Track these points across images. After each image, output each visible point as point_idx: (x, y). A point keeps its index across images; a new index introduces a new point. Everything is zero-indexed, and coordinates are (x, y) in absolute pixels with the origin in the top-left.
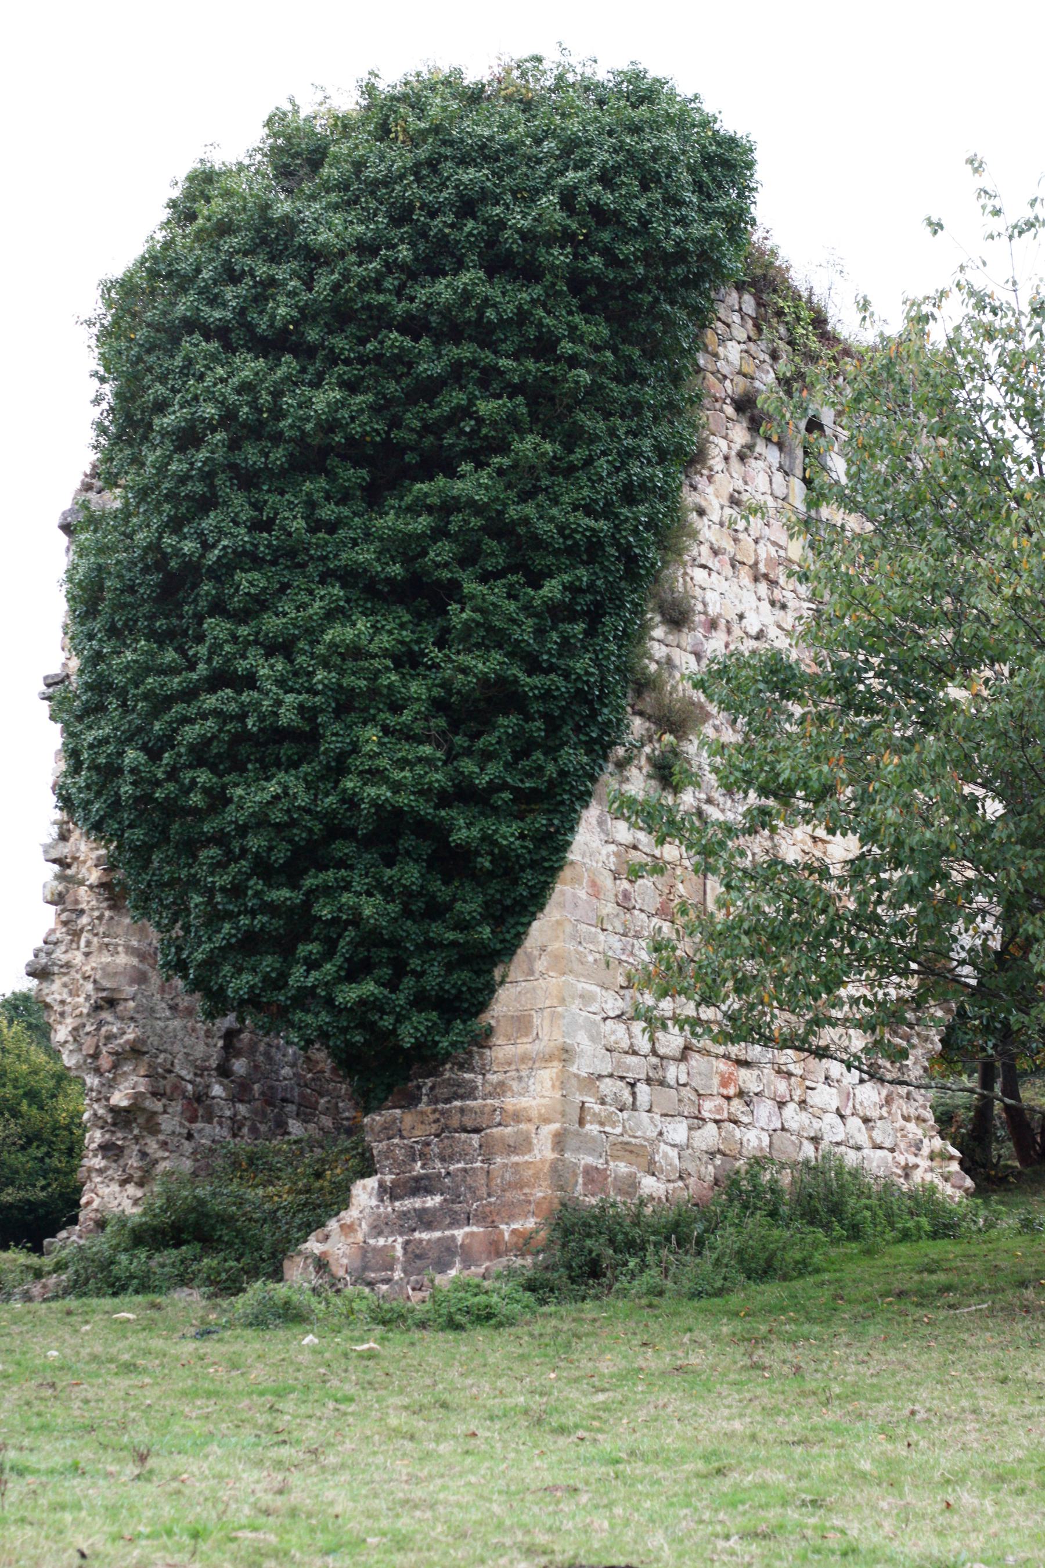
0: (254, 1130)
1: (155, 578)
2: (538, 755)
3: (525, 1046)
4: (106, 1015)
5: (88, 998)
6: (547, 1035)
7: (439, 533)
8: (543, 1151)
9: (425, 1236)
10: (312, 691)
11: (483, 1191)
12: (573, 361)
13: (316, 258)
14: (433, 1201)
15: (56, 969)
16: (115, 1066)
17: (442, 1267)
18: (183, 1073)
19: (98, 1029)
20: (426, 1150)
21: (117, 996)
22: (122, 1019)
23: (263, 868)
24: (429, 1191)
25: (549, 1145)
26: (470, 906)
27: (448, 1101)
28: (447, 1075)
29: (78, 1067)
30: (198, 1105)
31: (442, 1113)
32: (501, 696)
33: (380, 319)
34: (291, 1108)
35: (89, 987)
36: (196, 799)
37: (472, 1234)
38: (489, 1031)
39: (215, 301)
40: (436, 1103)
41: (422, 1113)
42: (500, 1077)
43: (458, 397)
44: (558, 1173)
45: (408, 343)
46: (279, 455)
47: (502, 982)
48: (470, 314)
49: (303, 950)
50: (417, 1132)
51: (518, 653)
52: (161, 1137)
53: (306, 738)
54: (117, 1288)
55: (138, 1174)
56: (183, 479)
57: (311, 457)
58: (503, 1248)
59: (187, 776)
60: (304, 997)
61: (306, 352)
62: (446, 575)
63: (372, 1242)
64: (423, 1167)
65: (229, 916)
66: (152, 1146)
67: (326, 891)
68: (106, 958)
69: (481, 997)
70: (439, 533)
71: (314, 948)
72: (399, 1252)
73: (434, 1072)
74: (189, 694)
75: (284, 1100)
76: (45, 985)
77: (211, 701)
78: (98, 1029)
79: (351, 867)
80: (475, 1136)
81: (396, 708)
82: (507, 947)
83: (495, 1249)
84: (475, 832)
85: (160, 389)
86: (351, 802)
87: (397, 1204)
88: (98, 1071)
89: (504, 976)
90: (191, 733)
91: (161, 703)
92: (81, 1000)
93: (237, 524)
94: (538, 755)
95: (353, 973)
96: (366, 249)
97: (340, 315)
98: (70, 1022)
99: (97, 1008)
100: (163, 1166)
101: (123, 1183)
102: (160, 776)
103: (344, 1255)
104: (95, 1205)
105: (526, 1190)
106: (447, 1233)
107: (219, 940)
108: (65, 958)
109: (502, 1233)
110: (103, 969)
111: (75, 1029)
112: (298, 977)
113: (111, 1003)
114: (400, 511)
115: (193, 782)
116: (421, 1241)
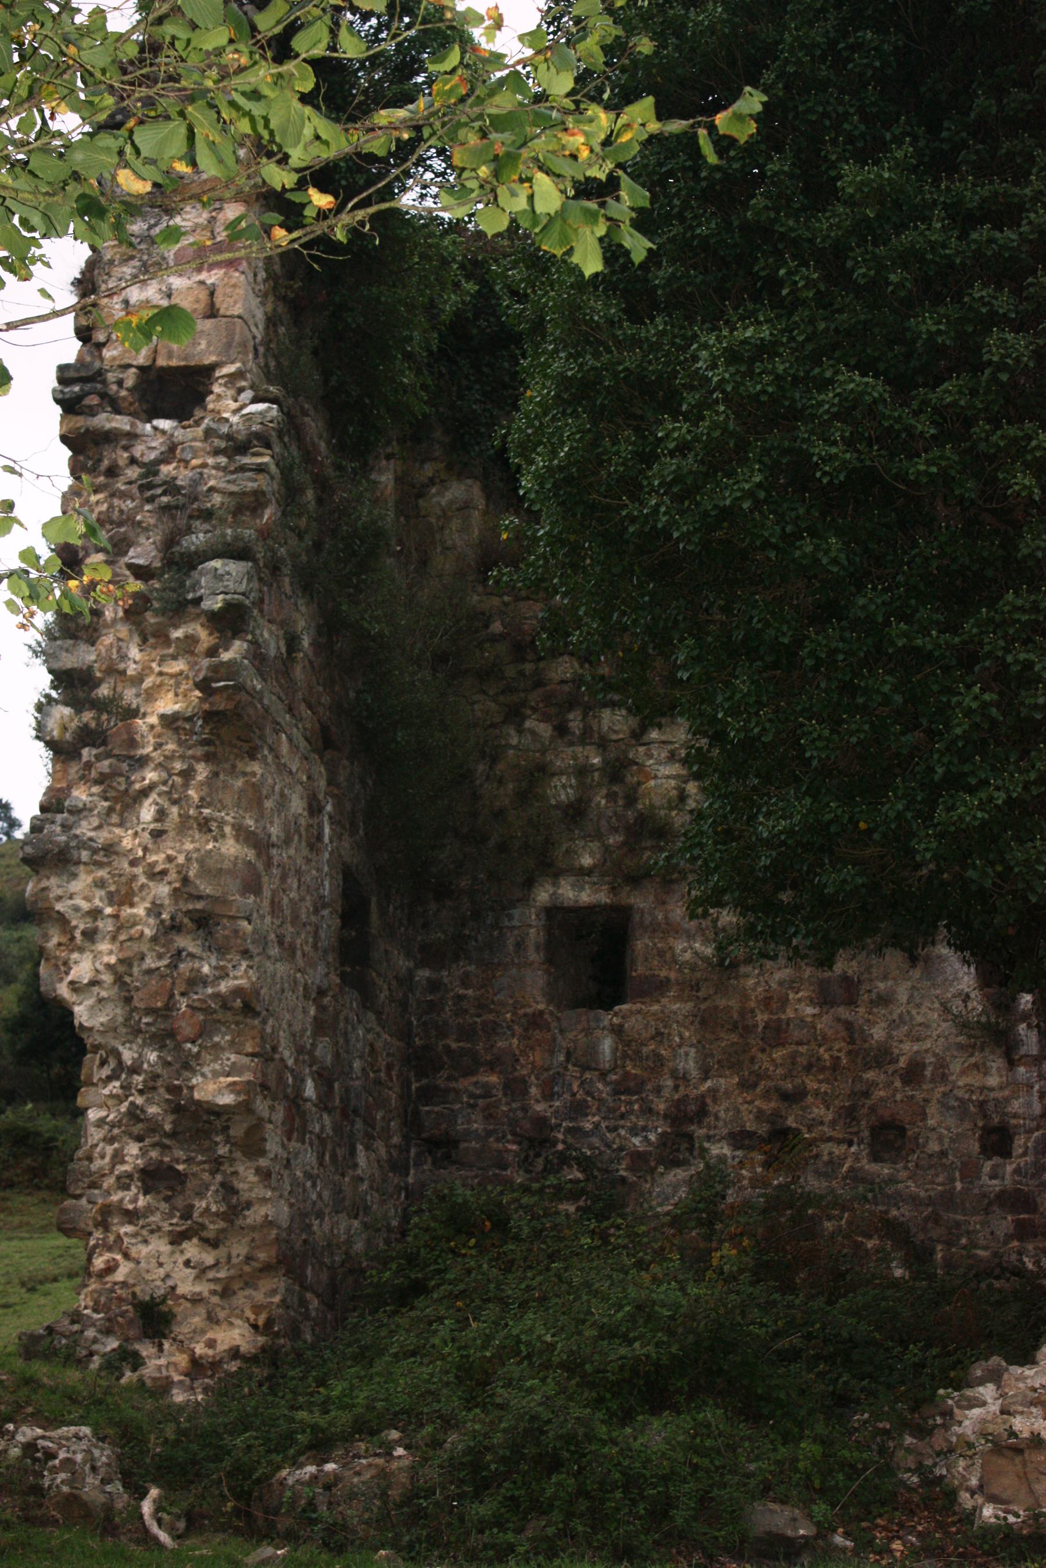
4: (187, 943)
5: (155, 910)
15: (85, 855)
16: (203, 1032)
21: (219, 909)
22: (222, 951)
29: (111, 1029)
35: (163, 890)
52: (263, 1162)
55: (213, 1227)
78: (173, 966)
88: (164, 1038)
98: (107, 952)
100: (255, 1215)
101: (177, 1239)
104: (120, 1275)
108: (103, 837)
110: (201, 861)
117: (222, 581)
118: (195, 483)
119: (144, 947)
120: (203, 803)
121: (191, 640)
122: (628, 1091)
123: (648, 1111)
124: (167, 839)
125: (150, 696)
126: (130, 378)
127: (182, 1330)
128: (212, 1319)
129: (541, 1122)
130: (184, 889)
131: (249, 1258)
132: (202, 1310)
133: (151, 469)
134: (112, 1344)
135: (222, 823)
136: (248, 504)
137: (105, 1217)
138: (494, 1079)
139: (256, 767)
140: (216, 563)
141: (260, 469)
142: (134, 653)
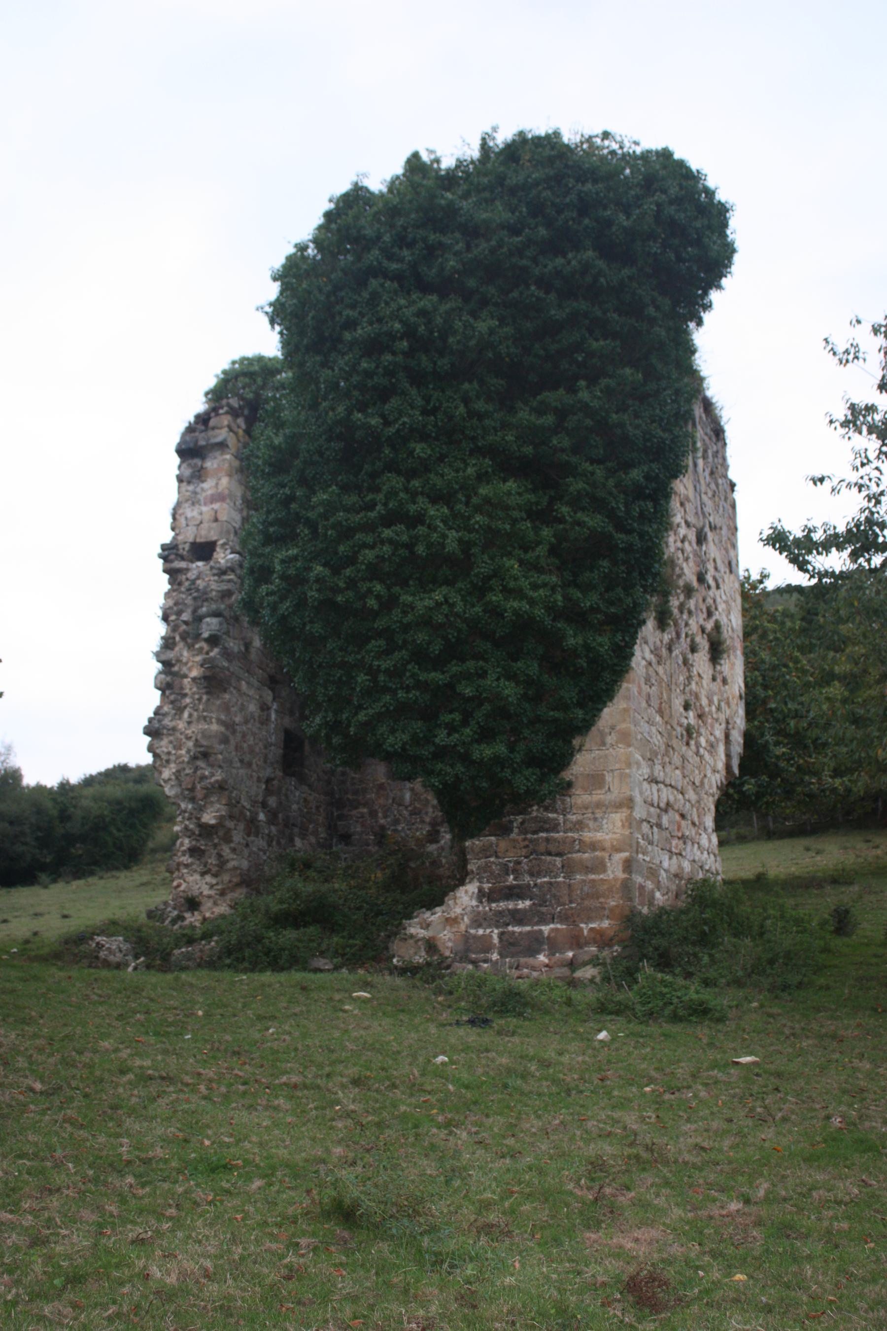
0: (279, 843)
1: (336, 445)
3: (598, 796)
4: (201, 763)
5: (188, 751)
6: (615, 790)
8: (614, 871)
9: (517, 929)
10: (470, 530)
11: (566, 899)
12: (652, 321)
13: (473, 232)
14: (523, 904)
15: (165, 731)
16: (206, 797)
17: (533, 952)
18: (245, 804)
19: (195, 772)
20: (518, 867)
22: (212, 766)
23: (420, 656)
24: (521, 897)
25: (620, 868)
26: (570, 694)
27: (535, 832)
28: (534, 814)
29: (177, 796)
30: (252, 826)
31: (531, 841)
34: (296, 830)
35: (190, 744)
36: (372, 603)
37: (557, 929)
38: (570, 785)
39: (390, 257)
40: (526, 833)
41: (514, 840)
42: (580, 817)
44: (626, 886)
45: (542, 295)
47: (580, 750)
49: (446, 718)
50: (509, 854)
51: (611, 515)
52: (232, 845)
54: (276, 961)
55: (215, 869)
58: (582, 941)
59: (364, 587)
60: (441, 753)
62: (564, 457)
63: (472, 931)
64: (515, 879)
65: (386, 690)
66: (226, 851)
68: (204, 726)
69: (564, 759)
71: (457, 716)
72: (496, 940)
74: (369, 527)
75: (293, 825)
76: (155, 741)
77: (387, 533)
78: (195, 772)
79: (486, 660)
80: (558, 859)
82: (585, 726)
83: (577, 942)
84: (580, 640)
85: (348, 312)
86: (496, 612)
87: (494, 905)
88: (193, 800)
89: (581, 746)
90: (369, 555)
91: (346, 533)
92: (183, 752)
93: (412, 408)
94: (619, 590)
95: (486, 735)
96: (515, 231)
98: (173, 767)
99: (195, 758)
100: (231, 865)
101: (203, 874)
102: (342, 585)
103: (450, 940)
104: (182, 888)
105: (602, 900)
106: (535, 928)
107: (377, 707)
109: (582, 930)
111: (178, 771)
112: (442, 737)
113: (205, 755)
115: (370, 591)
116: (514, 932)
117: (210, 626)
118: (206, 587)
119: (185, 765)
120: (204, 711)
121: (201, 649)
122: (415, 814)
123: (423, 822)
125: (190, 669)
126: (187, 547)
127: (203, 908)
128: (215, 904)
129: (383, 828)
130: (197, 744)
131: (230, 881)
132: (211, 901)
133: (193, 582)
134: (176, 913)
135: (211, 718)
138: (365, 810)
139: (227, 696)
140: (208, 619)
141: (229, 581)
142: (185, 653)
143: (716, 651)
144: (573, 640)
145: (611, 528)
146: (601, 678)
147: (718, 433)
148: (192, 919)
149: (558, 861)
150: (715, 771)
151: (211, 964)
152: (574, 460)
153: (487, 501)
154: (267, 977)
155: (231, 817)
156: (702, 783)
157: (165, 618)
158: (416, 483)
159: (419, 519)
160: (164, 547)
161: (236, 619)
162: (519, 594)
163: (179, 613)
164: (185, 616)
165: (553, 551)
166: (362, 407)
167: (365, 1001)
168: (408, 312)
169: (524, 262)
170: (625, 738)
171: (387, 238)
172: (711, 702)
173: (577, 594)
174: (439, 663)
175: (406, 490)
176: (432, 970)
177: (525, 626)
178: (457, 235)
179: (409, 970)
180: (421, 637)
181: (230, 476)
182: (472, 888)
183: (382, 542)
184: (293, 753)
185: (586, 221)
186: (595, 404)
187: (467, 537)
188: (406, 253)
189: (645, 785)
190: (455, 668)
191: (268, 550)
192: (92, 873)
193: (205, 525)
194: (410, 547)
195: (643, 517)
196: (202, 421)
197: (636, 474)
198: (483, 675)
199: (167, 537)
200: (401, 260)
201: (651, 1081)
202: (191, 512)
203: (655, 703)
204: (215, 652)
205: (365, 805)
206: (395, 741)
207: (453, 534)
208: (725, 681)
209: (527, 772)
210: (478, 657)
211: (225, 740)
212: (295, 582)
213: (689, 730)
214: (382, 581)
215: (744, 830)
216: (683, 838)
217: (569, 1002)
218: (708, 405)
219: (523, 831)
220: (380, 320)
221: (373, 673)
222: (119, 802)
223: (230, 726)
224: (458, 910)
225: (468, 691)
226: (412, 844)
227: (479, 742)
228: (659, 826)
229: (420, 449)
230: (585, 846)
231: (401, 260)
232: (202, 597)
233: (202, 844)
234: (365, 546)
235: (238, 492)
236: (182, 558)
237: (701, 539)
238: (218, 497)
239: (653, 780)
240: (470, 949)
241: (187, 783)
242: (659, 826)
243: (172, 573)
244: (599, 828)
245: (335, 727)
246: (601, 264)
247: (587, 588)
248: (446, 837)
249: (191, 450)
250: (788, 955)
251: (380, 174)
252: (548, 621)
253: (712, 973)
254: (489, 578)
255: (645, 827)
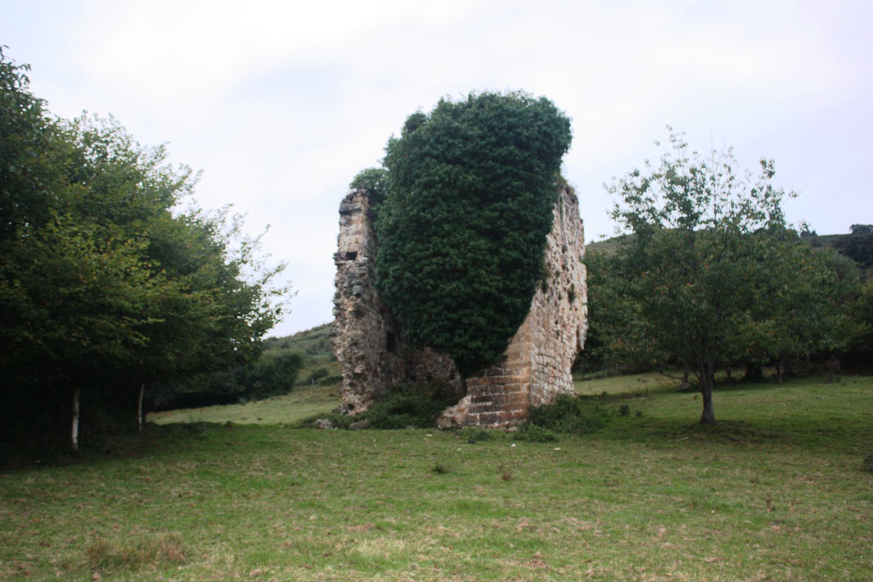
1: (414, 224)
2: (525, 281)
3: (518, 361)
4: (353, 347)
6: (524, 359)
7: (501, 217)
8: (524, 390)
9: (487, 413)
12: (538, 173)
13: (466, 139)
14: (489, 404)
17: (492, 422)
23: (448, 308)
24: (488, 401)
26: (506, 321)
32: (517, 263)
33: (485, 157)
35: (349, 339)
36: (429, 287)
38: (506, 357)
39: (433, 148)
43: (507, 180)
44: (528, 396)
46: (455, 192)
48: (512, 158)
49: (458, 332)
51: (522, 251)
53: (464, 272)
54: (391, 426)
56: (426, 197)
57: (464, 194)
60: (457, 345)
61: (463, 164)
65: (435, 321)
66: (365, 384)
67: (466, 315)
68: (354, 332)
69: (504, 347)
70: (501, 217)
71: (462, 331)
72: (478, 417)
73: (488, 367)
74: (427, 258)
77: (434, 260)
81: (489, 265)
82: (512, 334)
83: (510, 418)
86: (477, 291)
88: (351, 363)
90: (427, 269)
91: (418, 260)
95: (473, 338)
96: (483, 138)
97: (474, 155)
99: (351, 345)
100: (367, 390)
107: (431, 328)
114: (490, 210)
115: (428, 283)
117: (357, 289)
124: (349, 332)
129: (430, 373)
130: (352, 339)
136: (362, 275)
137: (345, 391)
143: (571, 297)
144: (507, 301)
145: (521, 257)
146: (519, 315)
147: (574, 200)
148: (352, 413)
149: (502, 387)
150: (571, 348)
151: (367, 427)
152: (507, 229)
153: (473, 247)
154: (392, 431)
155: (367, 370)
156: (564, 354)
157: (336, 285)
158: (445, 240)
159: (447, 255)
160: (335, 255)
161: (367, 286)
162: (486, 284)
163: (342, 283)
164: (345, 285)
165: (499, 265)
166: (424, 210)
167: (431, 438)
168: (440, 172)
169: (487, 151)
170: (528, 339)
171: (432, 141)
172: (569, 319)
173: (508, 283)
174: (455, 310)
175: (441, 243)
176: (454, 428)
177: (488, 295)
178: (460, 140)
179: (445, 429)
180: (448, 301)
181: (362, 223)
182: (469, 397)
183: (433, 264)
184: (391, 342)
185: (511, 133)
186: (514, 208)
187: (465, 261)
188: (439, 146)
189: (537, 357)
190: (461, 312)
191: (386, 265)
192: (267, 397)
193: (352, 245)
194: (443, 265)
195: (534, 252)
196: (350, 198)
197: (531, 235)
198: (472, 315)
199: (336, 250)
200: (437, 150)
201: (524, 454)
202: (345, 238)
203: (541, 323)
204: (359, 300)
205: (422, 363)
206: (439, 340)
207: (460, 261)
208: (576, 309)
209: (490, 352)
210: (470, 308)
211: (364, 338)
212: (398, 279)
213: (558, 333)
214: (433, 279)
215: (611, 371)
216: (555, 377)
217: (504, 437)
218: (569, 190)
219: (489, 375)
220: (430, 175)
221: (430, 314)
222: (279, 359)
223: (366, 331)
224: (464, 406)
225: (466, 321)
226: (443, 381)
227: (471, 341)
228: (543, 372)
229: (447, 227)
230: (512, 381)
231: (437, 150)
232: (353, 276)
233: (355, 382)
234: (426, 265)
235: (366, 229)
236: (343, 259)
237: (564, 250)
238: (358, 233)
239: (540, 354)
240: (468, 420)
241: (348, 356)
242: (543, 372)
243: (339, 266)
244: (518, 374)
245: (415, 335)
246: (517, 151)
247: (512, 280)
248: (458, 377)
249: (345, 213)
250: (589, 421)
251: (428, 108)
252: (497, 294)
253: (560, 428)
254: (474, 277)
255: (537, 373)
